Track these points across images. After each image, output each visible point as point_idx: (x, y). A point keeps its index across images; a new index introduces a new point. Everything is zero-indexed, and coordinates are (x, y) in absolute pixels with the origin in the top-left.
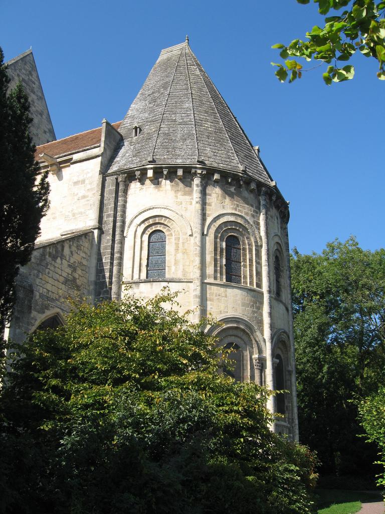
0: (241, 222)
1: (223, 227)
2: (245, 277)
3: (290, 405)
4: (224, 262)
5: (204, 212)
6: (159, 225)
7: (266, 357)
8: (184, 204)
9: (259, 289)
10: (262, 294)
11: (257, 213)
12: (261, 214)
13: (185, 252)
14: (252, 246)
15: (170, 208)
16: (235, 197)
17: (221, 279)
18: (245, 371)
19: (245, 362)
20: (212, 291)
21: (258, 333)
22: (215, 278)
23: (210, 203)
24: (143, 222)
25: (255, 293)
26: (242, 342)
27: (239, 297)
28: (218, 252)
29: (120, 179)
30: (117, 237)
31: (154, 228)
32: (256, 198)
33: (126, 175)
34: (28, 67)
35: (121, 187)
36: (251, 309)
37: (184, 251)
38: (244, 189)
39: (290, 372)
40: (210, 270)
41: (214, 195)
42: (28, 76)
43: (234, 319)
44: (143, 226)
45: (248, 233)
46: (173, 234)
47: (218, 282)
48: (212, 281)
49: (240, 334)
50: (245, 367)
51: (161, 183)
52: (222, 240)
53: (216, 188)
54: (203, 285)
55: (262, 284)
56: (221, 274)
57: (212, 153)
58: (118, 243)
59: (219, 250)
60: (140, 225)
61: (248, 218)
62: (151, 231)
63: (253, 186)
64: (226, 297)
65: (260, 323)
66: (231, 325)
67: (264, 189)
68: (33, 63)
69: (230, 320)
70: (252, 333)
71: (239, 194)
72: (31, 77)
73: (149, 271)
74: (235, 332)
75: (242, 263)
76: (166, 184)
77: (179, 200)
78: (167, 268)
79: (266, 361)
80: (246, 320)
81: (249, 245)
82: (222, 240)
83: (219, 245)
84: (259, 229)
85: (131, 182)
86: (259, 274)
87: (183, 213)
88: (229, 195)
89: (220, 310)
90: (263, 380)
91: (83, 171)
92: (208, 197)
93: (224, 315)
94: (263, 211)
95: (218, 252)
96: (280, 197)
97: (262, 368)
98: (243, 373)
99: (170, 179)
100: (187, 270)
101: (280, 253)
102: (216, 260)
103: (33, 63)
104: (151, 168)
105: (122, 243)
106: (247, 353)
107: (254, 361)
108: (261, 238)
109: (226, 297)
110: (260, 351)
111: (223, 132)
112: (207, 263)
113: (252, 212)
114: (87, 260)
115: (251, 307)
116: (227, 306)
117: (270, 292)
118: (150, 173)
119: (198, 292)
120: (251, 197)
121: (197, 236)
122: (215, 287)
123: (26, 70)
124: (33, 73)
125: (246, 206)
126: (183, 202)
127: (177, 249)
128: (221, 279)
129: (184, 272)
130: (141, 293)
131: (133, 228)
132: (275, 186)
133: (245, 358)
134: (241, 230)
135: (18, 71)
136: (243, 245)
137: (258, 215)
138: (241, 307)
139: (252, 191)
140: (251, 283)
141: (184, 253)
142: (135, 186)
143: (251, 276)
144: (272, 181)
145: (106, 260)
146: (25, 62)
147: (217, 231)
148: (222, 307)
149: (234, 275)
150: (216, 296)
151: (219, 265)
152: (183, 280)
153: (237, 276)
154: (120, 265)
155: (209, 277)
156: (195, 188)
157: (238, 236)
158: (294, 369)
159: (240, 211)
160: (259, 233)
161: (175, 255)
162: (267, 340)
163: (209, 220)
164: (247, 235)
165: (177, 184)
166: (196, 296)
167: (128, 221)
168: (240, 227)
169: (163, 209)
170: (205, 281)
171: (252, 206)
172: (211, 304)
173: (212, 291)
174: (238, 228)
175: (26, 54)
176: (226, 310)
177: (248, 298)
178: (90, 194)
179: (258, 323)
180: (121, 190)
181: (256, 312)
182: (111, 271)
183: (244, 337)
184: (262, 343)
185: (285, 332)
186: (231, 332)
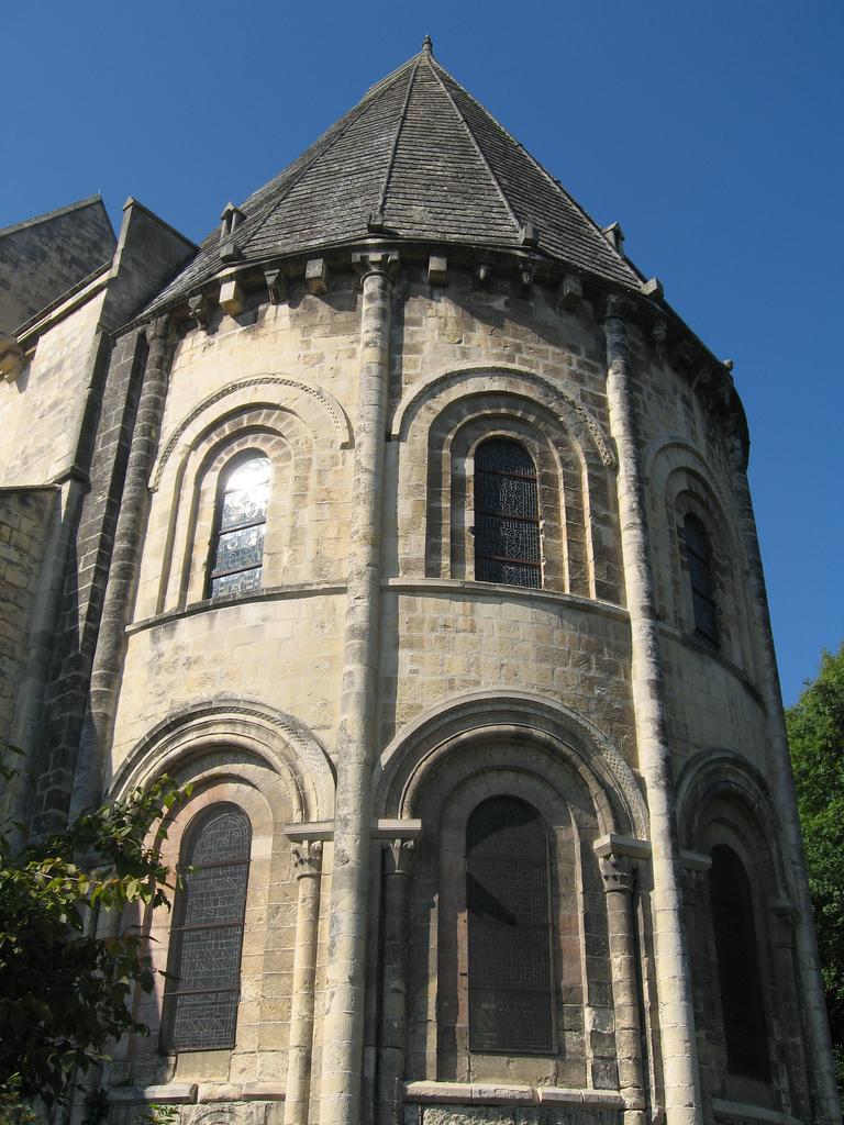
0: (531, 395)
1: (464, 411)
2: (554, 567)
3: (798, 1040)
4: (469, 518)
5: (396, 372)
6: (251, 437)
7: (648, 843)
11: (594, 370)
12: (610, 372)
14: (578, 466)
15: (287, 378)
16: (507, 322)
17: (456, 572)
18: (563, 903)
19: (561, 867)
20: (419, 613)
22: (432, 571)
23: (414, 346)
26: (550, 794)
27: (523, 630)
28: (446, 488)
29: (150, 333)
33: (165, 316)
34: (89, 232)
36: (580, 671)
37: (324, 495)
39: (788, 919)
40: (411, 545)
41: (430, 324)
42: (90, 252)
43: (506, 707)
45: (562, 427)
47: (444, 581)
48: (418, 578)
49: (540, 762)
50: (562, 882)
51: (264, 315)
52: (459, 450)
53: (439, 301)
54: (383, 598)
56: (457, 557)
58: (128, 509)
59: (447, 481)
60: (195, 446)
61: (558, 383)
63: (570, 286)
65: (623, 720)
66: (494, 728)
67: (613, 299)
70: (586, 759)
71: (523, 316)
74: (513, 756)
75: (541, 523)
76: (278, 316)
77: (313, 351)
79: (649, 858)
80: (556, 707)
81: (565, 464)
82: (459, 450)
83: (446, 467)
85: (183, 337)
86: (608, 556)
87: (325, 386)
88: (485, 320)
89: (448, 676)
90: (641, 933)
91: (64, 339)
92: (408, 329)
93: (464, 692)
94: (616, 363)
95: (446, 488)
96: (679, 333)
97: (636, 884)
98: (556, 907)
99: (290, 298)
100: (329, 553)
101: (704, 504)
102: (433, 516)
104: (230, 278)
106: (570, 835)
107: (601, 861)
108: (610, 443)
110: (623, 822)
111: (495, 193)
113: (574, 368)
114: (28, 573)
115: (576, 665)
117: (653, 612)
119: (360, 617)
121: (366, 442)
122: (431, 601)
123: (84, 239)
125: (551, 348)
126: (327, 355)
128: (456, 572)
129: (319, 567)
130: (178, 649)
132: (658, 295)
133: (562, 850)
134: (532, 419)
135: (59, 241)
136: (541, 466)
137: (600, 377)
138: (533, 665)
139: (570, 306)
140: (578, 583)
141: (321, 503)
142: (193, 344)
143: (577, 562)
144: (645, 282)
145: (86, 566)
148: (457, 664)
149: (511, 564)
151: (446, 530)
152: (314, 588)
153: (523, 565)
154: (130, 573)
155: (407, 569)
156: (365, 306)
158: (803, 904)
159: (524, 362)
160: (606, 430)
161: (294, 514)
162: (649, 782)
163: (409, 393)
164: (557, 435)
166: (352, 632)
168: (526, 411)
170: (392, 582)
171: (574, 349)
172: (413, 660)
173: (417, 614)
174: (519, 414)
175: (84, 204)
176: (473, 676)
177: (563, 634)
178: (69, 393)
179: (611, 721)
180: (155, 362)
181: (601, 683)
182: (97, 596)
183: (554, 773)
184: (631, 794)
185: (739, 762)
186: (498, 757)
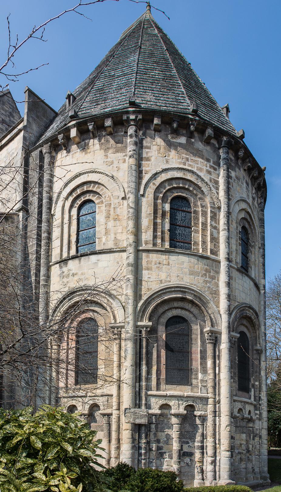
0: (191, 179)
1: (167, 185)
4: (167, 226)
5: (141, 169)
8: (116, 162)
9: (214, 257)
10: (219, 262)
13: (117, 219)
14: (206, 208)
15: (98, 170)
19: (193, 336)
21: (212, 304)
24: (70, 194)
25: (208, 261)
30: (44, 216)
31: (83, 199)
32: (214, 151)
35: (47, 160)
38: (197, 139)
40: (147, 236)
41: (155, 148)
44: (71, 199)
46: (104, 201)
49: (188, 306)
52: (164, 200)
54: (138, 252)
55: (219, 251)
56: (163, 240)
57: (154, 98)
59: (160, 212)
60: (67, 198)
61: (201, 174)
62: (79, 203)
64: (168, 265)
65: (216, 293)
66: (175, 296)
67: (225, 138)
68: (13, 105)
69: (173, 289)
72: (12, 119)
73: (79, 248)
74: (180, 304)
76: (94, 144)
77: (109, 160)
78: (97, 240)
81: (202, 207)
83: (160, 207)
84: (217, 189)
92: (145, 151)
101: (248, 222)
102: (155, 224)
103: (13, 105)
105: (49, 222)
107: (206, 335)
109: (168, 265)
112: (143, 227)
116: (169, 275)
118: (73, 133)
119: (131, 260)
120: (206, 149)
121: (131, 198)
124: (14, 114)
126: (114, 161)
127: (108, 217)
130: (69, 270)
131: (60, 203)
134: (191, 189)
139: (207, 142)
146: (3, 102)
147: (158, 190)
150: (155, 264)
152: (115, 250)
157: (187, 196)
159: (190, 165)
160: (218, 193)
161: (106, 224)
165: (108, 141)
167: (55, 196)
169: (90, 174)
170: (141, 248)
171: (208, 160)
174: (187, 187)
176: (168, 279)
181: (210, 282)
183: (194, 310)
185: (250, 307)
